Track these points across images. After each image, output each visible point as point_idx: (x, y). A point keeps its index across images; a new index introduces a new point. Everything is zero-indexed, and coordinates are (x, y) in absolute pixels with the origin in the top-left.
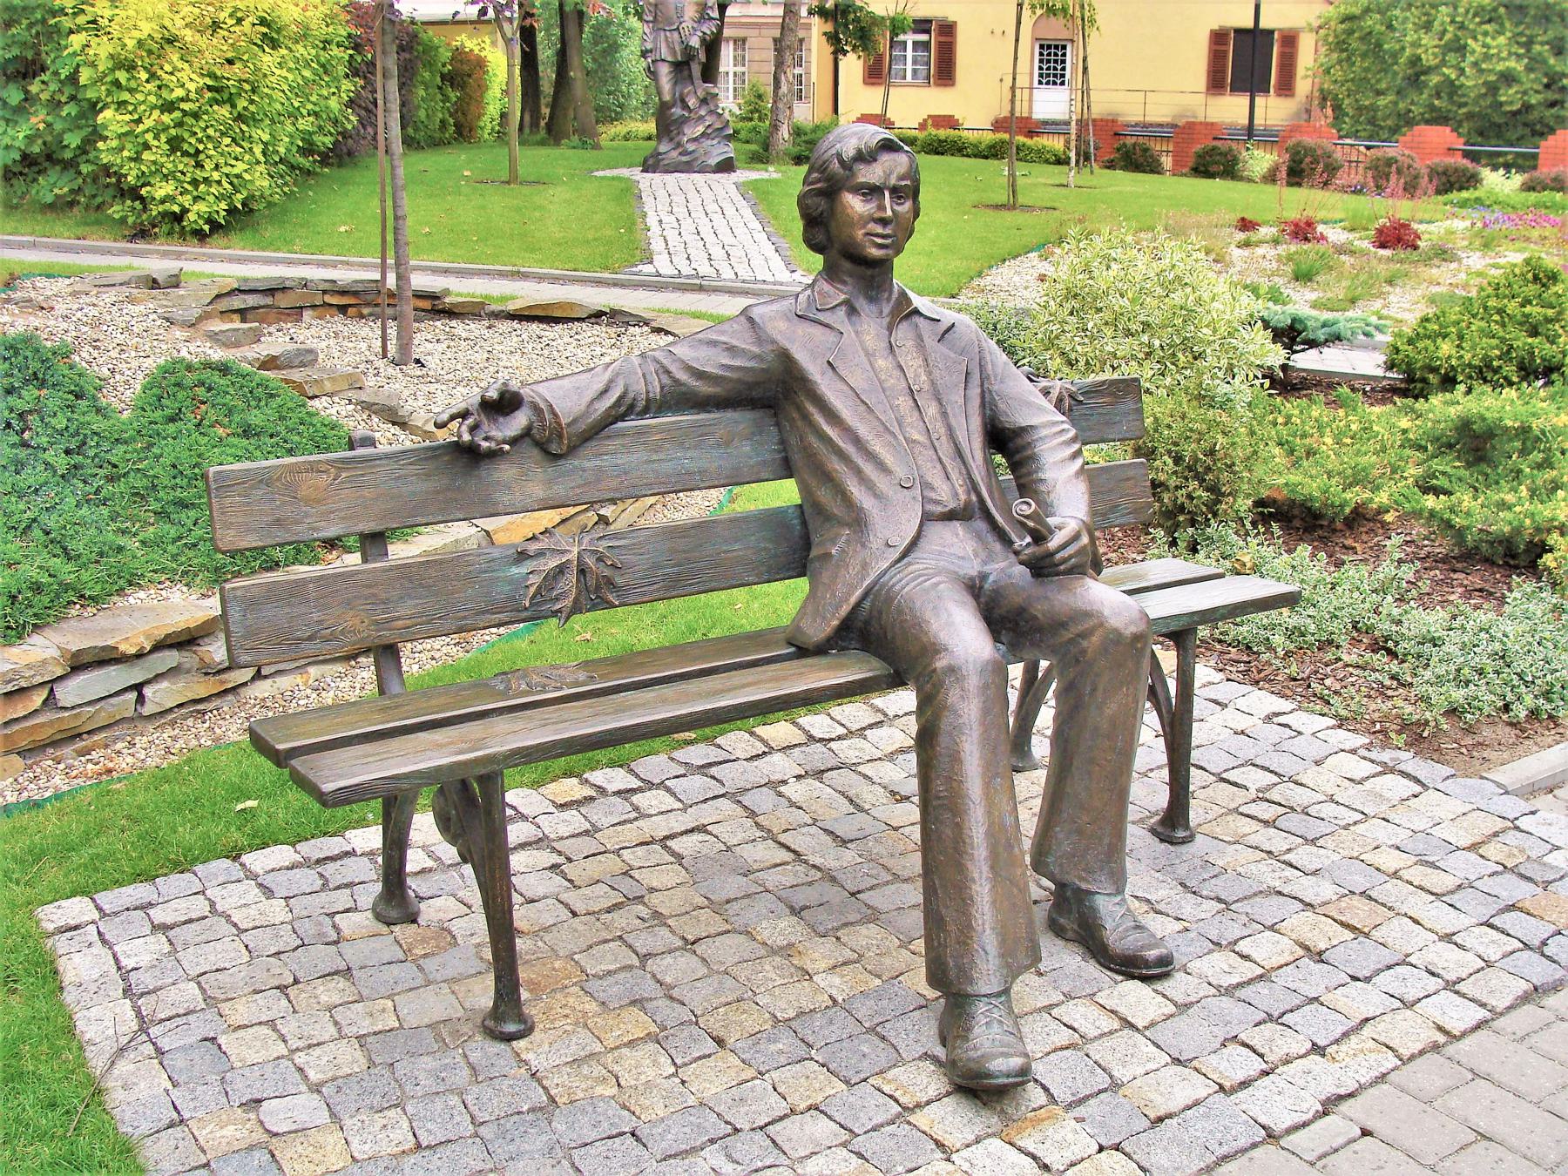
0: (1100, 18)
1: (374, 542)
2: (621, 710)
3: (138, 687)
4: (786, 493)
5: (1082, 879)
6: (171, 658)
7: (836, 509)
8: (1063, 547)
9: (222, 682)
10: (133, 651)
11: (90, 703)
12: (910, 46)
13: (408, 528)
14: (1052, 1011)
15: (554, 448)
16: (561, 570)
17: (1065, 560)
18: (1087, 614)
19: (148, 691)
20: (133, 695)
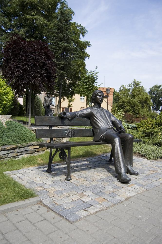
0: (122, 184)
1: (51, 127)
2: (79, 141)
3: (8, 154)
4: (91, 128)
5: (127, 165)
6: (12, 151)
7: (98, 127)
8: (123, 130)
9: (17, 154)
10: (8, 149)
11: (2, 155)
12: (82, 98)
13: (54, 126)
14: (123, 85)
15: (70, 119)
16: (70, 132)
17: (123, 131)
18: (126, 137)
19: (9, 154)
20: (7, 155)
